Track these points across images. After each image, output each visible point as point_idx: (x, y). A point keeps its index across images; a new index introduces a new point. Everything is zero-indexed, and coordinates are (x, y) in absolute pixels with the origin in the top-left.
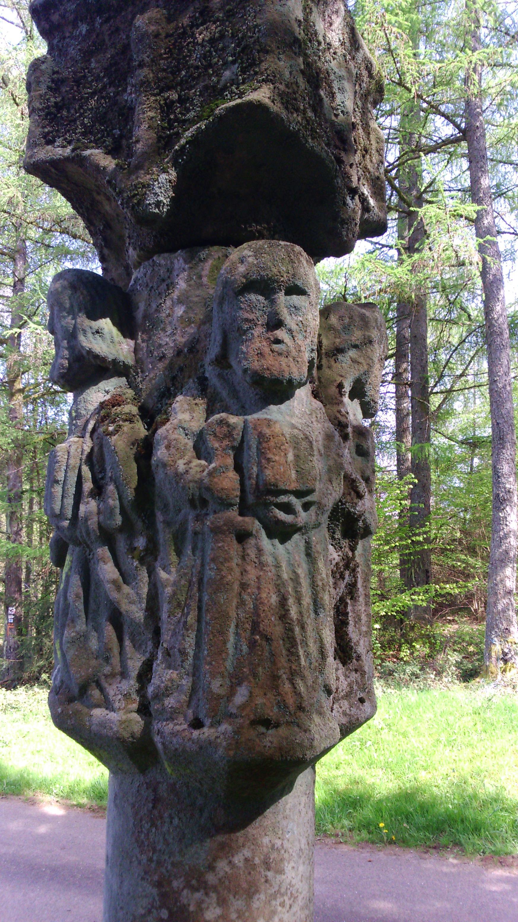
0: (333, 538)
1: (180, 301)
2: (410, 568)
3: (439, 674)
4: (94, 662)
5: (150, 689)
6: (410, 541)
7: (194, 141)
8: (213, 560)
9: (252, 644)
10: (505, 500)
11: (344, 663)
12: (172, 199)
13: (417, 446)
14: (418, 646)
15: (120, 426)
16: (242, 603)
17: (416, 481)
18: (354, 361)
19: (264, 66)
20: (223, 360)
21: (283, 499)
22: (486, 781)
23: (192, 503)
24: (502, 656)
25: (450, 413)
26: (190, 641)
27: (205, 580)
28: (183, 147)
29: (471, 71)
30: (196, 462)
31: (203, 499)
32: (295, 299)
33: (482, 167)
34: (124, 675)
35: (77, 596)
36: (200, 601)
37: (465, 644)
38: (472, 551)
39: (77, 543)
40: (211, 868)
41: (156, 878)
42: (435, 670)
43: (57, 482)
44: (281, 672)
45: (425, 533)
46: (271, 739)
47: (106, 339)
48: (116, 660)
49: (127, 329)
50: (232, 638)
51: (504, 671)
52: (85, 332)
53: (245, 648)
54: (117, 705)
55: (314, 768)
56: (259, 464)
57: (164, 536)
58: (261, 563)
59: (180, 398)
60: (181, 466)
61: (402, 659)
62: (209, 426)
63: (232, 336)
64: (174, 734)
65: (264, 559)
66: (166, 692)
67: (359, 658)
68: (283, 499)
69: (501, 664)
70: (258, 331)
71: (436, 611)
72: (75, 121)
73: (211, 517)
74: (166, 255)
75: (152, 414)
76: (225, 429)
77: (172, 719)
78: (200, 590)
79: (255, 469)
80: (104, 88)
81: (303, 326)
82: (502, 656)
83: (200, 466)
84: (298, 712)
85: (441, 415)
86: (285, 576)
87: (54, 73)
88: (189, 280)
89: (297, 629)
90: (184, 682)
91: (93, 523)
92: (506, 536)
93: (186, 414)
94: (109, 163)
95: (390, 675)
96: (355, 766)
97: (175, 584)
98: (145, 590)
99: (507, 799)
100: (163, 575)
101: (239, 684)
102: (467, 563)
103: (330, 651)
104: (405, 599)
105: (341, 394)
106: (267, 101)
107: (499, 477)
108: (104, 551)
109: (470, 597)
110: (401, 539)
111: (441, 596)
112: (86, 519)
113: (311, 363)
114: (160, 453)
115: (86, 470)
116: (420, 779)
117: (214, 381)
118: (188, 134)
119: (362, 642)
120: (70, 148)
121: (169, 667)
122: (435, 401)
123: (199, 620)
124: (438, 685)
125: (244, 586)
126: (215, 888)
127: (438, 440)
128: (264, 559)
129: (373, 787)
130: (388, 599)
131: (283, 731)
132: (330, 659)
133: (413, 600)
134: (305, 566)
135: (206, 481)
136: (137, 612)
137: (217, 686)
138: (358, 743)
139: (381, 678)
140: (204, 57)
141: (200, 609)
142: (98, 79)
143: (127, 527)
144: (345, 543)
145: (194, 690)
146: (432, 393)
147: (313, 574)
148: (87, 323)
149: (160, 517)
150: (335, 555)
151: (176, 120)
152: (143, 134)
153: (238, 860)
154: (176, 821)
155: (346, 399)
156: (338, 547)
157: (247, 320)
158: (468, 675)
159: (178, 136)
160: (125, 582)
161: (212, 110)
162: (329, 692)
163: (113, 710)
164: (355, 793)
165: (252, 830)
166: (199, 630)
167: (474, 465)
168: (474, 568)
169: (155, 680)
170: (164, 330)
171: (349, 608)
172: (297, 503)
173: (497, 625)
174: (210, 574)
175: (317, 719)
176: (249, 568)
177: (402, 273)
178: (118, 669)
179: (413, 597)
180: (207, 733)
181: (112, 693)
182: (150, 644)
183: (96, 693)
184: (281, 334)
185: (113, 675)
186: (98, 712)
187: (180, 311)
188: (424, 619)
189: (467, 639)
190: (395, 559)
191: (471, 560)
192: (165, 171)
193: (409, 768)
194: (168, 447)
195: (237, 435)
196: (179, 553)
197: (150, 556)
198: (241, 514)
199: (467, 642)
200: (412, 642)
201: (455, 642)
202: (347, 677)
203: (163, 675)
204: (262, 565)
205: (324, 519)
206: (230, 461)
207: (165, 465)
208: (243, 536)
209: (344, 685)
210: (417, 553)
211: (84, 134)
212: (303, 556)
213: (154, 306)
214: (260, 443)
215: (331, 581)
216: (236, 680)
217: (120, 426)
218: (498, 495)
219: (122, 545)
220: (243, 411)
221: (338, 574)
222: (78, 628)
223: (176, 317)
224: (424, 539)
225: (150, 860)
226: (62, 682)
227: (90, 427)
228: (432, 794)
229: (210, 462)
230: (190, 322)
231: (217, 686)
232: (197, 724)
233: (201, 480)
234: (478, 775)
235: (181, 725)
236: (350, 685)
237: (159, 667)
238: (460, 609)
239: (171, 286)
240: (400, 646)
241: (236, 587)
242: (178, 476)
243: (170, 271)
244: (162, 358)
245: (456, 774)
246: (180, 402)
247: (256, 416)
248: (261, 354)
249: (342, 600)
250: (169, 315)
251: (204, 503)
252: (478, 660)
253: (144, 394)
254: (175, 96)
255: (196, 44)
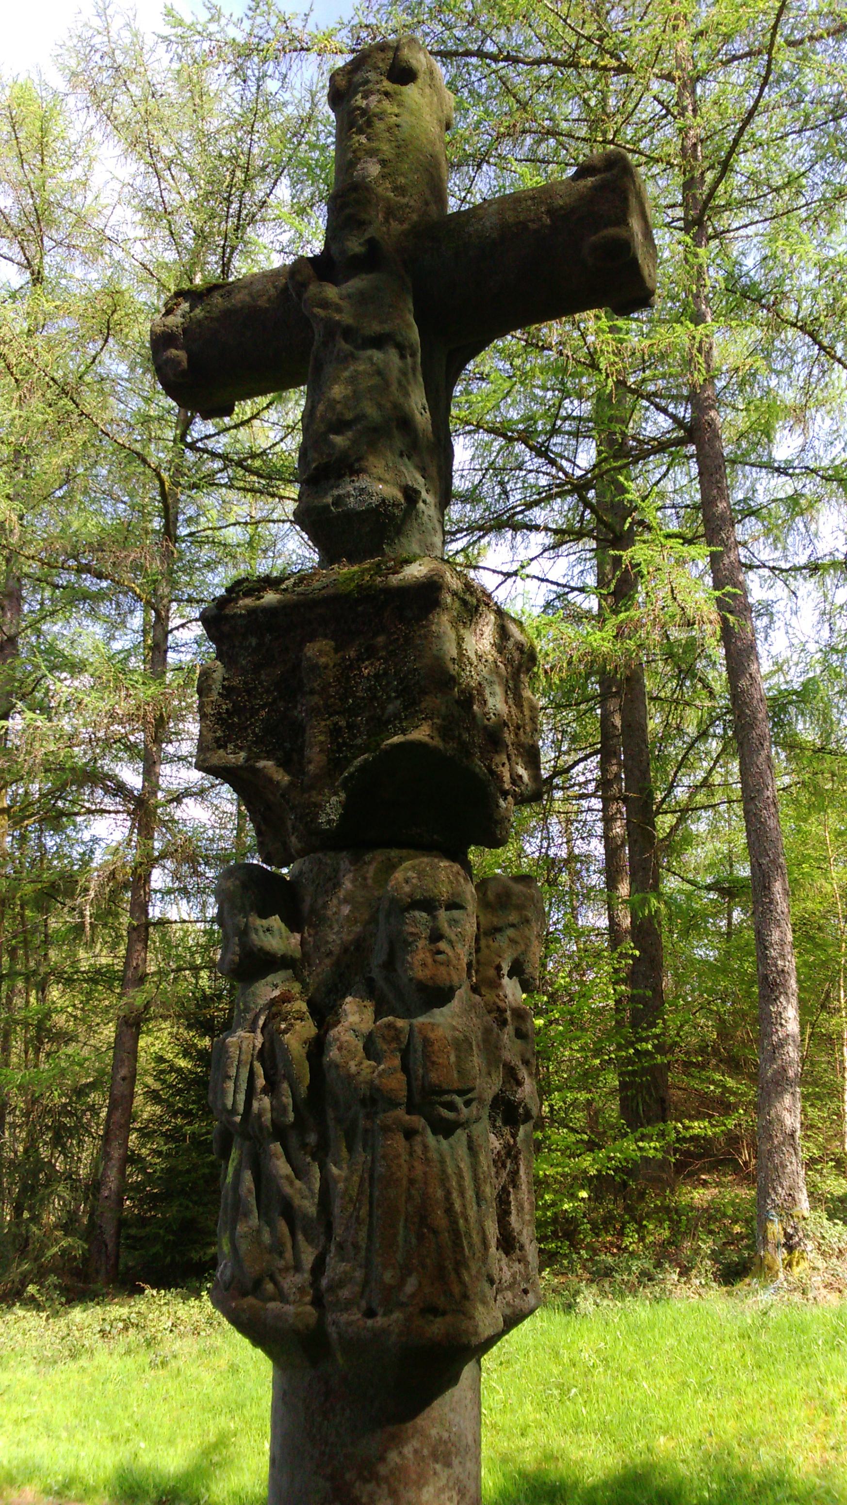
0: (494, 1126)
1: (346, 901)
2: (634, 1097)
3: (685, 1272)
4: (267, 1257)
5: (324, 1282)
6: (631, 1051)
7: (362, 769)
8: (384, 1157)
9: (421, 1237)
10: (777, 985)
11: (507, 1254)
12: (341, 815)
13: (637, 897)
14: (651, 1227)
15: (292, 1025)
16: (410, 1198)
17: (637, 953)
18: (512, 941)
19: (423, 705)
20: (390, 965)
21: (447, 1098)
22: (762, 1450)
23: (363, 1102)
24: (783, 1241)
25: (688, 840)
26: (363, 1234)
27: (376, 1176)
28: (352, 775)
29: (695, 351)
30: (368, 1063)
31: (375, 1099)
32: (456, 913)
33: (718, 482)
34: (297, 1268)
35: (249, 1191)
36: (371, 1196)
37: (727, 1222)
38: (734, 1065)
39: (246, 1136)
40: (382, 1459)
41: (329, 1470)
42: (679, 1265)
43: (229, 1077)
44: (447, 1263)
45: (657, 1036)
46: (437, 1328)
47: (275, 935)
48: (289, 1255)
49: (294, 923)
50: (401, 1231)
51: (790, 1265)
52: (256, 930)
53: (414, 1241)
54: (292, 1298)
55: (478, 1362)
56: (424, 1066)
57: (336, 1133)
58: (427, 1159)
59: (349, 999)
60: (353, 1067)
61: (626, 1247)
62: (379, 1028)
63: (398, 947)
64: (349, 1324)
65: (429, 1155)
66: (341, 1284)
67: (522, 1248)
68: (447, 1098)
69: (783, 1253)
70: (421, 943)
71: (680, 1167)
72: (246, 728)
73: (381, 1116)
74: (332, 854)
75: (324, 1013)
76: (392, 1033)
77: (347, 1309)
78: (371, 1185)
79: (421, 1071)
80: (275, 701)
81: (461, 936)
82: (783, 1241)
83: (370, 1066)
84: (462, 1304)
85: (677, 842)
86: (450, 1171)
87: (224, 679)
88: (354, 881)
89: (461, 1221)
90: (357, 1274)
91: (267, 1117)
92: (781, 1044)
93: (355, 1015)
94: (282, 777)
95: (607, 1275)
96: (552, 1430)
97: (347, 1179)
98: (317, 1185)
99: (796, 1482)
100: (335, 1170)
101: (410, 1274)
102: (724, 1086)
103: (493, 1243)
104: (629, 1148)
105: (500, 976)
106: (427, 739)
107: (766, 948)
108: (276, 1147)
109: (733, 1140)
110: (620, 1047)
111: (684, 1140)
112: (260, 1115)
113: (469, 965)
114: (334, 1054)
115: (257, 1065)
116: (657, 1450)
117: (381, 983)
118: (357, 762)
119: (525, 1232)
120: (243, 754)
121: (343, 1261)
122: (665, 822)
123: (370, 1215)
124: (683, 1290)
125: (412, 1182)
126: (386, 1479)
127: (671, 884)
128: (429, 1155)
129: (580, 1464)
130: (600, 1148)
131: (449, 1318)
132: (493, 1250)
133: (641, 1149)
134: (467, 1159)
135: (377, 1082)
136: (309, 1206)
137: (388, 1277)
138: (556, 1392)
139: (592, 1281)
140: (369, 689)
141: (371, 1204)
142: (268, 691)
143: (300, 1124)
144: (506, 1130)
145: (366, 1282)
146: (658, 813)
147: (475, 1166)
148: (259, 922)
149: (331, 1114)
150: (496, 1143)
151: (345, 744)
152: (315, 759)
153: (408, 1450)
154: (348, 1412)
155: (506, 980)
156: (499, 1135)
157: (412, 934)
158: (733, 1273)
159: (349, 761)
160: (297, 1177)
161: (379, 745)
162: (491, 1281)
163: (288, 1302)
164: (552, 1476)
165: (420, 1421)
166: (371, 1224)
167: (734, 921)
168: (734, 1094)
169: (329, 1273)
170: (331, 927)
171: (512, 1197)
172: (459, 1100)
173: (774, 1189)
174: (381, 1170)
175: (481, 1308)
176: (416, 1164)
177: (601, 640)
178: (292, 1263)
179: (641, 1144)
180: (380, 1321)
181: (286, 1286)
182: (322, 1238)
183: (270, 1287)
184: (443, 945)
185: (287, 1269)
186: (271, 1305)
187: (346, 910)
188: (660, 1180)
189: (730, 1212)
190: (613, 1080)
191: (731, 1083)
192: (336, 794)
193: (638, 1431)
194: (340, 1049)
195: (404, 1039)
196: (350, 1149)
197: (321, 1152)
198: (408, 1113)
199: (730, 1217)
200: (642, 1219)
201: (711, 1216)
202: (510, 1267)
203: (336, 1267)
204: (427, 1161)
205: (485, 1113)
206: (397, 1062)
207: (337, 1066)
208: (410, 1134)
209: (507, 1275)
210: (645, 1071)
211: (255, 743)
212: (465, 1149)
213: (320, 902)
214: (425, 1046)
215: (493, 1170)
216: (406, 1271)
217: (292, 1025)
218: (766, 977)
219: (294, 1141)
220: (409, 1014)
221: (499, 1162)
222: (251, 1223)
223: (342, 914)
224: (654, 1046)
225: (323, 1454)
226: (233, 1277)
227: (261, 1022)
228: (675, 1475)
229: (379, 1064)
230: (356, 921)
231: (388, 1277)
232: (370, 1313)
233: (372, 1081)
234: (750, 1440)
235: (355, 1315)
236: (513, 1276)
237: (331, 1259)
238: (721, 1162)
239: (337, 885)
240: (623, 1227)
241: (405, 1182)
242: (350, 1077)
243: (336, 871)
244: (330, 954)
245: (715, 1440)
246: (350, 1004)
247: (421, 1019)
248: (424, 965)
249: (504, 1189)
250: (335, 913)
251: (374, 1101)
252: (747, 1247)
253: (311, 988)
254: (343, 723)
255: (362, 676)
